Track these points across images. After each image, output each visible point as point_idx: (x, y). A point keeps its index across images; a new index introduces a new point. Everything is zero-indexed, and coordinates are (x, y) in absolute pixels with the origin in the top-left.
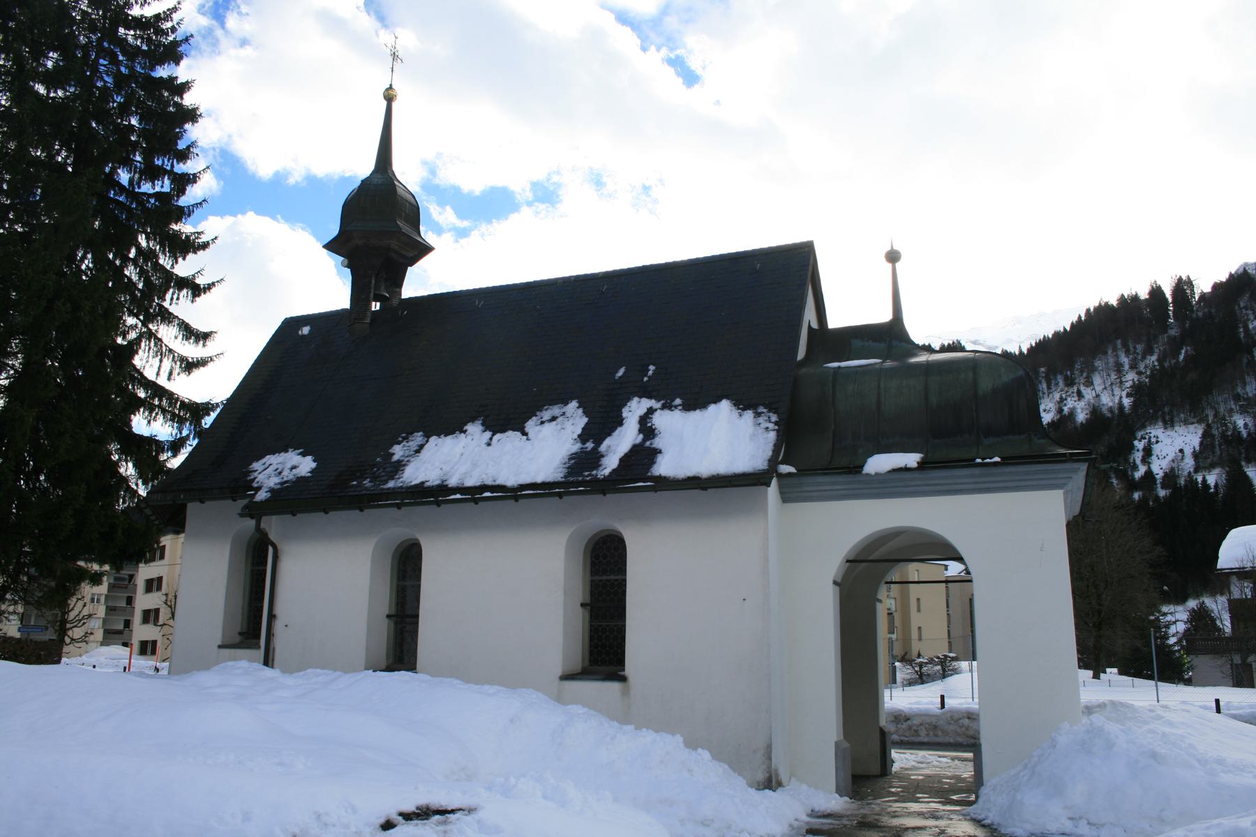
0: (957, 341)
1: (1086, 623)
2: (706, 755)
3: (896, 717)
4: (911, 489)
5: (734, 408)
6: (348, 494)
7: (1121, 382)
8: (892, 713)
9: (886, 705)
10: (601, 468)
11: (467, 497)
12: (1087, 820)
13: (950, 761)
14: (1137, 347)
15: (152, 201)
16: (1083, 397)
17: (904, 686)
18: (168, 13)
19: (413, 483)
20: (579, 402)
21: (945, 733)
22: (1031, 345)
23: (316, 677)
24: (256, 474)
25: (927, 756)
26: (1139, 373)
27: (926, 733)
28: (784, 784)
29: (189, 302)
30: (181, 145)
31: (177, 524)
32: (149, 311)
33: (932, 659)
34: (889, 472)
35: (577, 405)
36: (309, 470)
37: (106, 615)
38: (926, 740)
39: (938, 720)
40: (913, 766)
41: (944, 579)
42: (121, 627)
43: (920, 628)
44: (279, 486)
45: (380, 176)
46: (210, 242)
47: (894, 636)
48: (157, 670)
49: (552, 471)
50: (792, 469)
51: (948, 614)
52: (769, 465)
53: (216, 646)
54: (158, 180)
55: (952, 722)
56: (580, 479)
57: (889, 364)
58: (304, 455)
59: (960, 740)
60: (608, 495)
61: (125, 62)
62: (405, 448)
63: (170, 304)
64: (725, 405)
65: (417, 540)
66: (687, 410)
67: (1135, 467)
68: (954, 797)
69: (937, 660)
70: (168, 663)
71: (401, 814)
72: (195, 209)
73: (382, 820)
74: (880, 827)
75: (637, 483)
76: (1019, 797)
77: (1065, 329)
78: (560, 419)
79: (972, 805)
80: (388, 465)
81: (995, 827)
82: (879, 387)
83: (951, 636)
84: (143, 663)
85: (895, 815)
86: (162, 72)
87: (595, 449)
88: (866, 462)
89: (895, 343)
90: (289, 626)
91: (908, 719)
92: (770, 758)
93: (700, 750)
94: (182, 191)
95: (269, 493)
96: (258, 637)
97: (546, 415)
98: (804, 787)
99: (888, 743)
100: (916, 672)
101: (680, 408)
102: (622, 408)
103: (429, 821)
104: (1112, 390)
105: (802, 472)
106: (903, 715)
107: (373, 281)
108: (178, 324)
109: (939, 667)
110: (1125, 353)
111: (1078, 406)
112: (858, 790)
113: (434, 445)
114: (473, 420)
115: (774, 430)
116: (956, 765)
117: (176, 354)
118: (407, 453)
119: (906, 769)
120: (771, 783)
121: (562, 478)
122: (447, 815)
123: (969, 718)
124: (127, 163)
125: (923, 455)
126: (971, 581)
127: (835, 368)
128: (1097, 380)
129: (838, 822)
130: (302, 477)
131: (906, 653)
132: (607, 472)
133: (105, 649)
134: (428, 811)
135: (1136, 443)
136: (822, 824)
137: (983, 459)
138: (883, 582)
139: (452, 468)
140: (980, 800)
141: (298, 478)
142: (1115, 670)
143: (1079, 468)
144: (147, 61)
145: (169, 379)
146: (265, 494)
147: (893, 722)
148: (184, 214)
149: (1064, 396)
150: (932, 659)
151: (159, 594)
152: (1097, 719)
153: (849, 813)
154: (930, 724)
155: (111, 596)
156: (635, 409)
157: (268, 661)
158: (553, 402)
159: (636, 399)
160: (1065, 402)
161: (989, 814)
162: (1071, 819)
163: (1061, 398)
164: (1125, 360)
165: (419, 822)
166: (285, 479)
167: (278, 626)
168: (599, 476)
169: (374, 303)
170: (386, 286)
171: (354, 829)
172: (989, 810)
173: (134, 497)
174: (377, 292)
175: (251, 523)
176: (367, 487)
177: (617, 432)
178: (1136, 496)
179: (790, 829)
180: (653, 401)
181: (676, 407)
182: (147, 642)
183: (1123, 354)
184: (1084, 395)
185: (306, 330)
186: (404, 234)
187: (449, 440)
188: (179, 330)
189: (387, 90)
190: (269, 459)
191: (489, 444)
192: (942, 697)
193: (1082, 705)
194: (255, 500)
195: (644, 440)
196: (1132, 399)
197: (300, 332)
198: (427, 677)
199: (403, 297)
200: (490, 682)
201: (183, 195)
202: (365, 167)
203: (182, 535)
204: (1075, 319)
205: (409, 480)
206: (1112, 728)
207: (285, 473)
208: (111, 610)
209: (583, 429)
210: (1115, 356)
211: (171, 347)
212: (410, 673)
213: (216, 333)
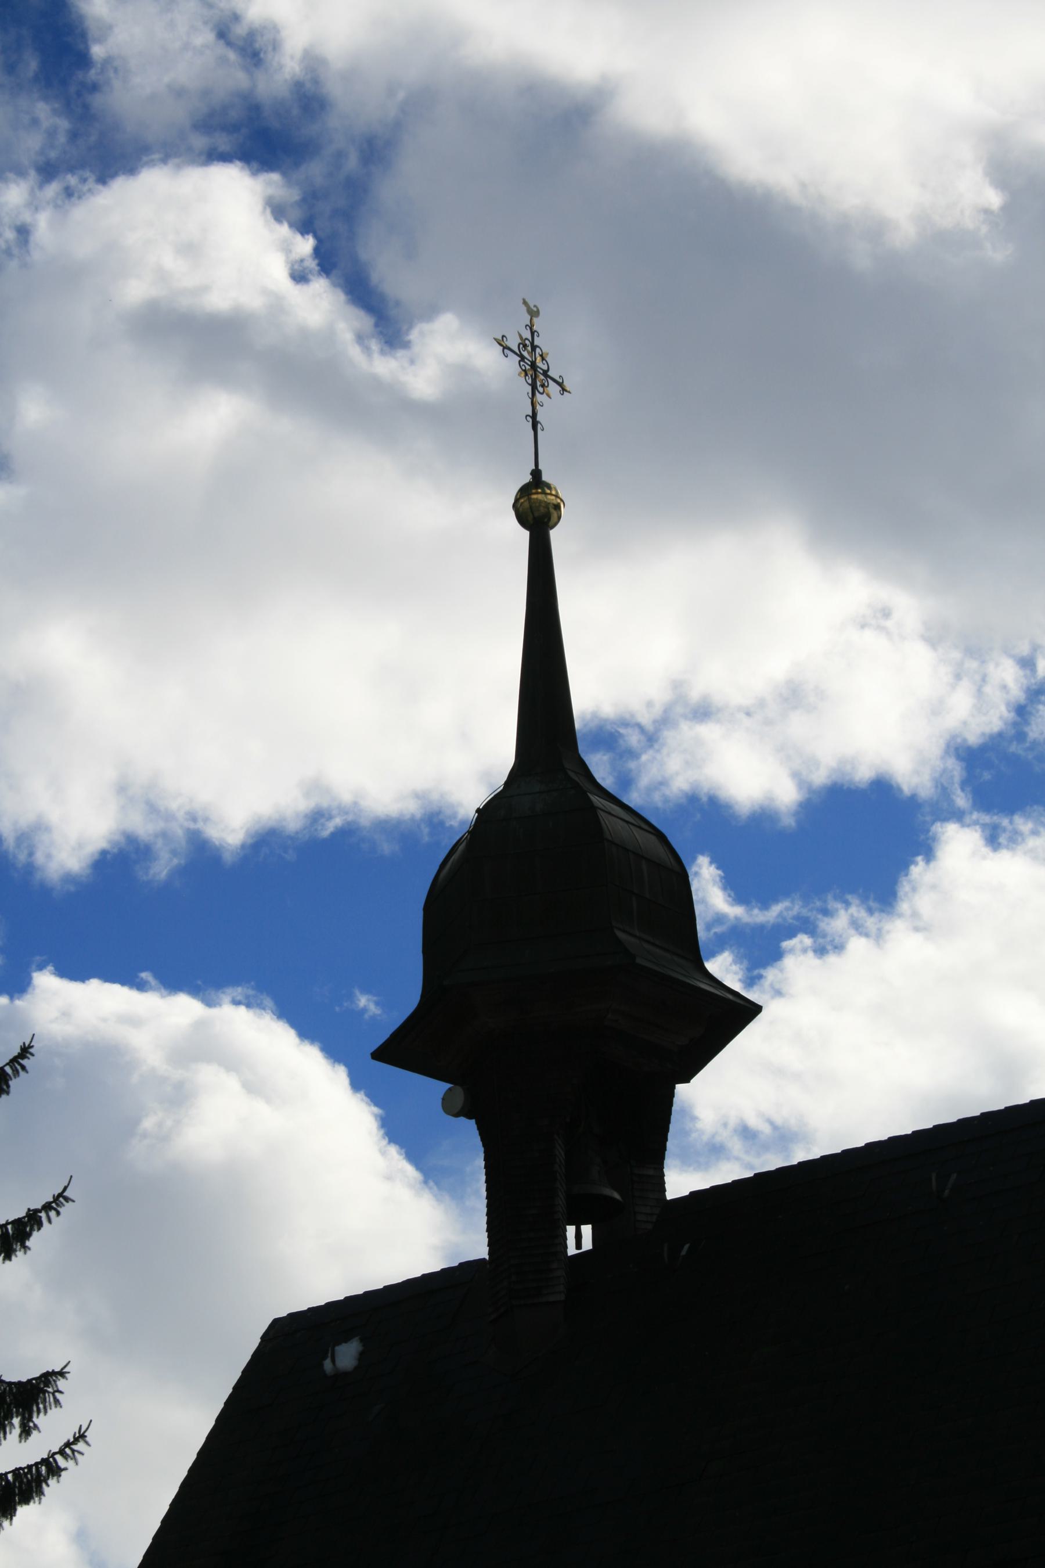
189: (525, 491)
197: (328, 1365)
199: (670, 1196)
213: (62, 1374)
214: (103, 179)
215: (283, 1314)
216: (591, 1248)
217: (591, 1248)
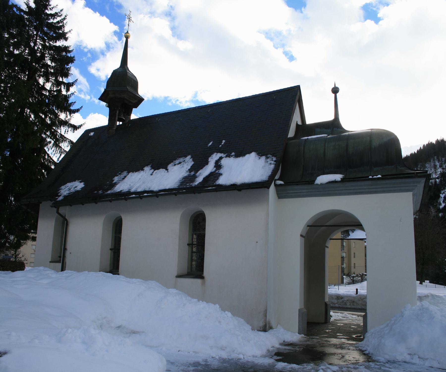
3: (337, 297)
5: (257, 155)
7: (436, 172)
8: (336, 295)
9: (328, 292)
10: (195, 182)
11: (137, 196)
12: (418, 355)
13: (357, 317)
18: (62, 20)
19: (117, 191)
20: (191, 156)
26: (443, 169)
27: (350, 304)
28: (274, 328)
29: (72, 133)
33: (358, 275)
34: (327, 183)
38: (349, 307)
39: (355, 299)
40: (340, 319)
50: (282, 182)
55: (360, 300)
58: (81, 182)
63: (65, 134)
64: (253, 154)
66: (236, 157)
67: (440, 204)
68: (354, 336)
69: (359, 275)
75: (208, 188)
77: (415, 152)
81: (370, 355)
82: (325, 146)
88: (316, 179)
91: (342, 298)
92: (266, 316)
93: (227, 312)
95: (63, 197)
97: (177, 162)
100: (351, 279)
101: (234, 156)
102: (209, 157)
105: (286, 184)
106: (340, 296)
108: (69, 142)
109: (360, 278)
110: (438, 161)
113: (130, 176)
114: (147, 165)
116: (359, 319)
120: (266, 328)
121: (177, 186)
125: (343, 176)
131: (349, 273)
132: (196, 183)
135: (441, 195)
136: (285, 349)
137: (373, 176)
138: (329, 239)
139: (134, 184)
140: (365, 340)
141: (76, 191)
142: (428, 281)
143: (421, 181)
150: (358, 275)
152: (425, 303)
154: (351, 300)
159: (215, 153)
161: (368, 348)
162: (409, 354)
164: (438, 164)
166: (71, 192)
168: (193, 185)
174: (119, 117)
177: (205, 167)
179: (267, 352)
180: (223, 154)
181: (232, 156)
183: (437, 162)
185: (92, 134)
186: (130, 92)
193: (418, 295)
195: (216, 170)
197: (90, 134)
201: (69, 91)
204: (419, 149)
205: (116, 190)
206: (433, 308)
209: (191, 167)
210: (434, 162)
211: (65, 150)
214: (113, 252)
215: (87, 129)
216: (133, 109)
217: (133, 109)
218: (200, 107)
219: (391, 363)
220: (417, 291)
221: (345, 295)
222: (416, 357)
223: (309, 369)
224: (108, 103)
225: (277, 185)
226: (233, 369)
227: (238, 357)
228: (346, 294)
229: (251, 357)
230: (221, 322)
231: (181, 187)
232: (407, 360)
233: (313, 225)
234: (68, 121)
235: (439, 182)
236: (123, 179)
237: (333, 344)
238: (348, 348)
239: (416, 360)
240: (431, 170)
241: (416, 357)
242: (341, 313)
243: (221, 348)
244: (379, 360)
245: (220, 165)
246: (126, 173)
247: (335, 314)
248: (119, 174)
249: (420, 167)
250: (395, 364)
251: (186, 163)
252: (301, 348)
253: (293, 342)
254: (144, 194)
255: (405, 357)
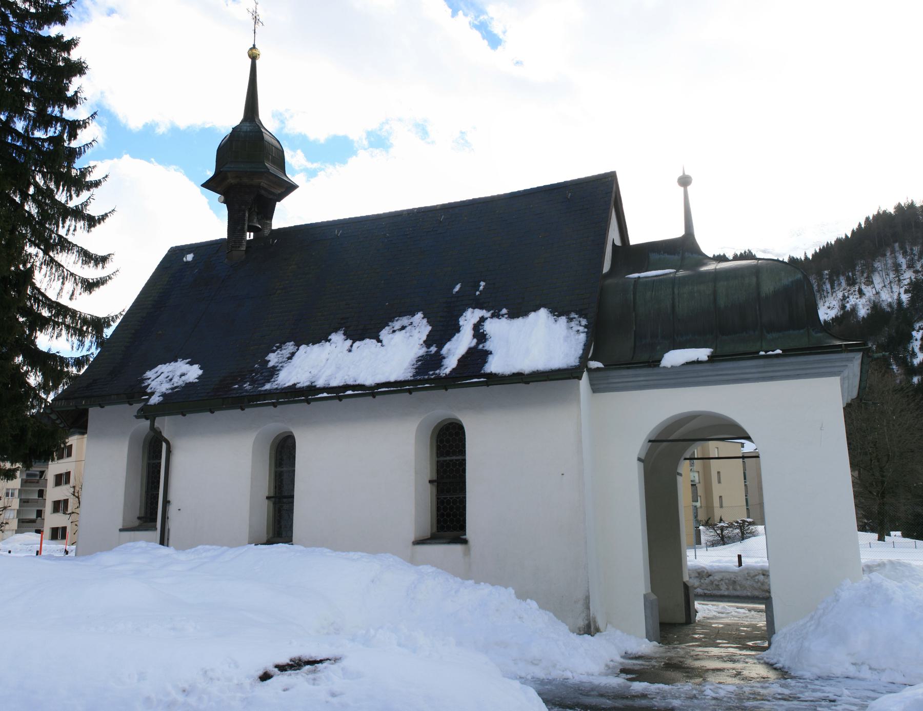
0: (748, 250)
1: (870, 492)
2: (533, 604)
3: (699, 573)
4: (701, 379)
5: (550, 315)
6: (230, 396)
7: (899, 280)
8: (696, 570)
10: (443, 368)
11: (333, 395)
12: (869, 665)
13: (747, 612)
14: (914, 249)
15: (46, 145)
16: (864, 294)
17: (707, 546)
19: (286, 385)
20: (423, 314)
21: (743, 587)
22: (816, 251)
23: (205, 552)
24: (149, 381)
25: (727, 607)
26: (916, 272)
27: (726, 587)
28: (601, 630)
29: (85, 232)
30: (70, 93)
31: (80, 425)
32: (49, 242)
35: (422, 316)
36: (197, 376)
37: (20, 506)
38: (726, 593)
39: (737, 576)
40: (715, 616)
41: (741, 455)
42: (34, 516)
43: (721, 497)
44: (170, 391)
45: (248, 125)
46: (102, 180)
47: (698, 504)
48: (67, 552)
49: (402, 371)
50: (600, 365)
51: (745, 485)
52: (580, 362)
53: (118, 530)
54: (52, 127)
55: (749, 578)
56: (426, 377)
57: (681, 273)
58: (191, 363)
59: (756, 593)
60: (449, 390)
61: (15, 23)
62: (279, 356)
64: (543, 312)
65: (292, 432)
66: (511, 318)
68: (750, 643)
69: (736, 524)
70: (75, 546)
71: (277, 666)
72: (86, 149)
73: (261, 673)
74: (684, 668)
76: (806, 644)
77: (846, 236)
78: (408, 329)
79: (765, 651)
80: (264, 370)
81: (786, 670)
82: (673, 293)
83: (749, 503)
84: (54, 547)
85: (697, 658)
86: (52, 30)
87: (438, 352)
89: (687, 254)
90: (180, 511)
91: (710, 575)
92: (588, 608)
93: (529, 601)
94: (73, 135)
95: (161, 397)
96: (155, 520)
97: (397, 325)
98: (619, 632)
99: (691, 596)
101: (506, 316)
102: (459, 317)
103: (301, 670)
104: (891, 288)
106: (706, 571)
107: (247, 215)
108: (78, 251)
109: (738, 531)
110: (903, 254)
111: (860, 303)
112: (666, 635)
114: (336, 330)
115: (584, 332)
116: (753, 615)
117: (77, 277)
118: (281, 360)
119: (708, 618)
120: (590, 629)
121: (411, 377)
122: (316, 665)
123: (764, 575)
124: (21, 112)
126: (758, 457)
127: (635, 278)
128: (877, 279)
129: (647, 663)
130: (190, 383)
132: (448, 371)
133: (19, 536)
134: (300, 662)
135: (914, 333)
136: (634, 664)
137: (766, 352)
138: (683, 458)
139: (320, 371)
140: (773, 647)
141: (186, 383)
142: (899, 533)
143: (854, 358)
144: (36, 21)
145: (71, 299)
146: (158, 398)
147: (697, 577)
148: (77, 154)
149: (846, 294)
150: (732, 524)
151: (67, 486)
152: (876, 577)
153: (657, 655)
154: (729, 580)
155: (24, 490)
156: (469, 318)
157: (163, 541)
158: (402, 314)
159: (470, 310)
160: (848, 299)
162: (853, 664)
163: (844, 296)
164: (903, 261)
165: (293, 672)
166: (175, 385)
167: (172, 511)
168: (441, 375)
169: (248, 234)
170: (258, 218)
171: (235, 681)
172: (780, 655)
173: (42, 403)
174: (250, 224)
175: (147, 423)
176: (247, 390)
177: (455, 337)
178: (916, 380)
179: (606, 668)
180: (484, 311)
181: (503, 315)
182: (57, 528)
184: (865, 293)
185: (190, 257)
187: (316, 348)
188: (79, 257)
189: (251, 49)
190: (161, 368)
191: (350, 351)
192: (740, 557)
194: (149, 404)
195: (478, 344)
196: (910, 295)
197: (185, 259)
198: (302, 548)
200: (355, 549)
201: (74, 139)
202: (236, 117)
203: (86, 436)
204: (855, 227)
205: (282, 383)
206: (890, 585)
207: (176, 380)
208: (24, 502)
209: (428, 336)
210: (893, 257)
211: (72, 272)
212: (287, 545)
215: (174, 246)
218: (423, 210)
219: (823, 679)
220: (862, 557)
221: (715, 569)
222: (865, 668)
223: (688, 689)
224: (223, 195)
225: (591, 369)
226: (565, 693)
227: (563, 675)
228: (718, 566)
229: (584, 675)
230: (522, 618)
231: (419, 378)
232: (851, 675)
233: (657, 439)
234: (82, 208)
235: (908, 304)
236: (290, 358)
237: (714, 656)
238: (744, 661)
239: (866, 673)
240: (888, 275)
241: (865, 668)
242: (712, 605)
243: (532, 662)
244: (803, 676)
245: (483, 332)
246: (293, 346)
247: (703, 607)
248: (276, 347)
249: (860, 269)
250: (830, 681)
251: (415, 329)
252: (662, 662)
253: (642, 653)
254: (346, 392)
255: (847, 669)
